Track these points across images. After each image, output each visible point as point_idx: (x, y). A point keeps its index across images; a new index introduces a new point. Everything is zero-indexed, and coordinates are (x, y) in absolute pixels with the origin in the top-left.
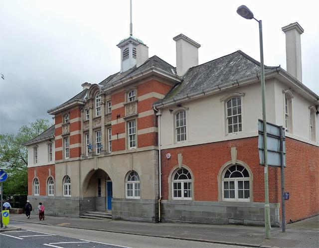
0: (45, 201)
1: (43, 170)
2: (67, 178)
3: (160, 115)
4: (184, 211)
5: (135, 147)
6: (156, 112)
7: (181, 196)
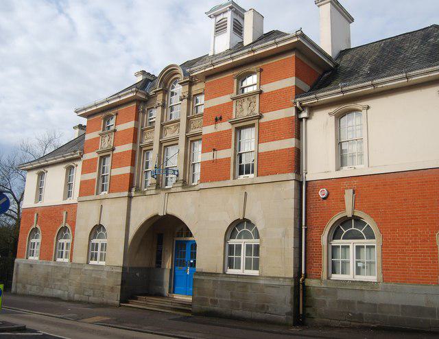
0: (50, 271)
1: (52, 213)
2: (98, 229)
3: (307, 119)
4: (360, 302)
5: (251, 176)
6: (298, 111)
7: (239, 268)
